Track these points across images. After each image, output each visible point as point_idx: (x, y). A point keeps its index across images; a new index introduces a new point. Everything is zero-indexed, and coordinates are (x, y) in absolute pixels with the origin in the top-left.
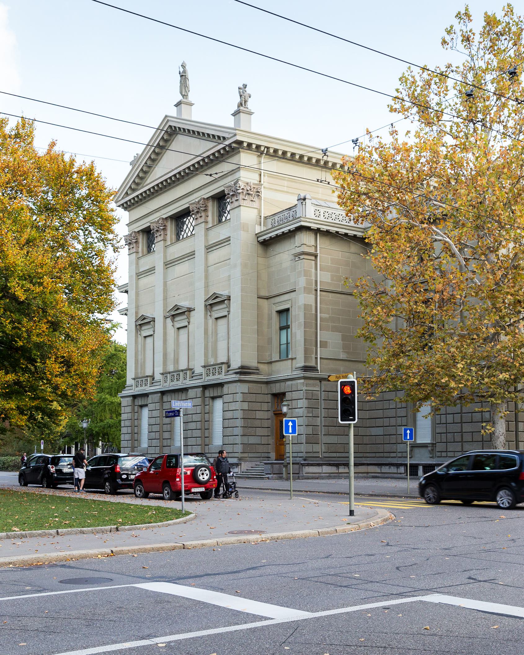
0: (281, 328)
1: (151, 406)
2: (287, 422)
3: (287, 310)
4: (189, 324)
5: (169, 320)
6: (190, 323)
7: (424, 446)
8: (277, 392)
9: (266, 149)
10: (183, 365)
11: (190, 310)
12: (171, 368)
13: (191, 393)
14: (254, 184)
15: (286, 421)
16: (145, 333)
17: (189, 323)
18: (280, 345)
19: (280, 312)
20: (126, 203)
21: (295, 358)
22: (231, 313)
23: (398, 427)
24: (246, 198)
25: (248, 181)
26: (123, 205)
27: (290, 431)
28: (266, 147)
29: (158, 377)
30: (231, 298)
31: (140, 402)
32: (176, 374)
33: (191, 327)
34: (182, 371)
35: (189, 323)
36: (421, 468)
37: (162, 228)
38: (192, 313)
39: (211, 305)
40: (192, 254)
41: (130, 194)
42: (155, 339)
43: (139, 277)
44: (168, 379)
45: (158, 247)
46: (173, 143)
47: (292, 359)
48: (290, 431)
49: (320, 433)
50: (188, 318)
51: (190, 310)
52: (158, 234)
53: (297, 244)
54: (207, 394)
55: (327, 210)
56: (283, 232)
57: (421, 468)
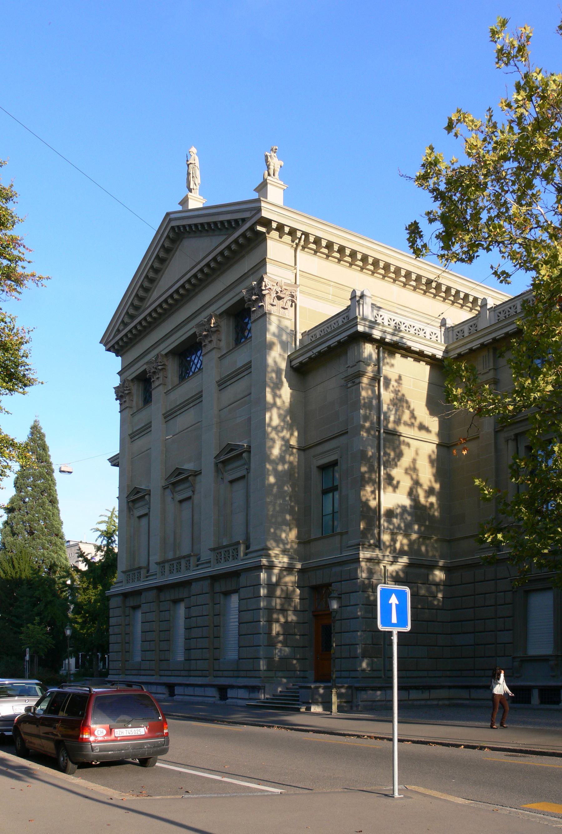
0: (325, 492)
1: (145, 607)
2: (387, 594)
3: (334, 464)
4: (194, 494)
5: (168, 491)
6: (196, 493)
7: (543, 659)
8: (318, 583)
9: (303, 236)
10: (185, 550)
11: (197, 474)
12: (170, 556)
13: (195, 588)
14: (287, 284)
15: (383, 590)
16: (138, 513)
17: (193, 491)
18: (323, 516)
19: (323, 468)
20: (117, 343)
21: (347, 533)
22: (252, 471)
23: (498, 633)
24: (274, 304)
25: (278, 279)
26: (113, 346)
27: (394, 620)
28: (304, 233)
29: (154, 568)
30: (252, 450)
31: (132, 602)
32: (175, 563)
33: (196, 498)
34: (184, 557)
35: (193, 491)
36: (535, 694)
37: (160, 367)
38: (198, 478)
39: (223, 462)
40: (198, 398)
41: (123, 330)
42: (151, 519)
43: (133, 439)
44: (166, 570)
45: (157, 393)
46: (177, 253)
47: (341, 534)
48: (394, 620)
49: (382, 643)
50: (193, 486)
51: (197, 474)
52: (155, 377)
53: (350, 363)
54: (218, 587)
55: (393, 318)
56: (329, 347)
57: (535, 694)
